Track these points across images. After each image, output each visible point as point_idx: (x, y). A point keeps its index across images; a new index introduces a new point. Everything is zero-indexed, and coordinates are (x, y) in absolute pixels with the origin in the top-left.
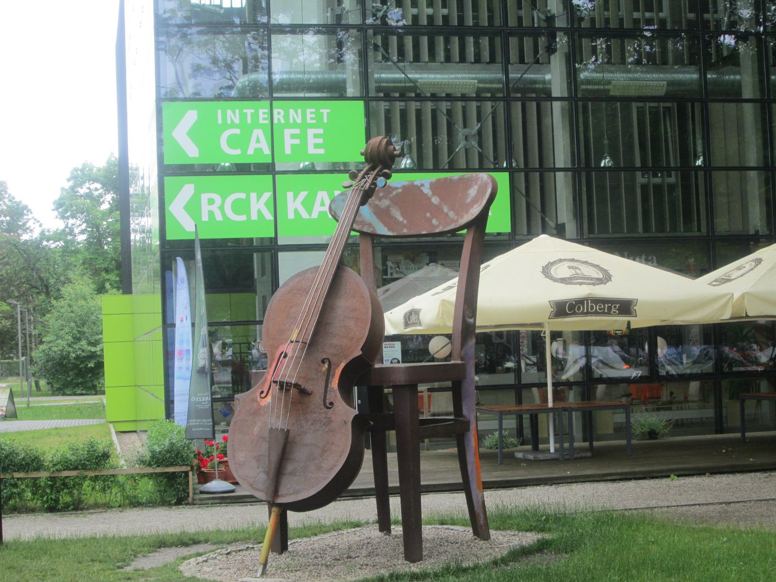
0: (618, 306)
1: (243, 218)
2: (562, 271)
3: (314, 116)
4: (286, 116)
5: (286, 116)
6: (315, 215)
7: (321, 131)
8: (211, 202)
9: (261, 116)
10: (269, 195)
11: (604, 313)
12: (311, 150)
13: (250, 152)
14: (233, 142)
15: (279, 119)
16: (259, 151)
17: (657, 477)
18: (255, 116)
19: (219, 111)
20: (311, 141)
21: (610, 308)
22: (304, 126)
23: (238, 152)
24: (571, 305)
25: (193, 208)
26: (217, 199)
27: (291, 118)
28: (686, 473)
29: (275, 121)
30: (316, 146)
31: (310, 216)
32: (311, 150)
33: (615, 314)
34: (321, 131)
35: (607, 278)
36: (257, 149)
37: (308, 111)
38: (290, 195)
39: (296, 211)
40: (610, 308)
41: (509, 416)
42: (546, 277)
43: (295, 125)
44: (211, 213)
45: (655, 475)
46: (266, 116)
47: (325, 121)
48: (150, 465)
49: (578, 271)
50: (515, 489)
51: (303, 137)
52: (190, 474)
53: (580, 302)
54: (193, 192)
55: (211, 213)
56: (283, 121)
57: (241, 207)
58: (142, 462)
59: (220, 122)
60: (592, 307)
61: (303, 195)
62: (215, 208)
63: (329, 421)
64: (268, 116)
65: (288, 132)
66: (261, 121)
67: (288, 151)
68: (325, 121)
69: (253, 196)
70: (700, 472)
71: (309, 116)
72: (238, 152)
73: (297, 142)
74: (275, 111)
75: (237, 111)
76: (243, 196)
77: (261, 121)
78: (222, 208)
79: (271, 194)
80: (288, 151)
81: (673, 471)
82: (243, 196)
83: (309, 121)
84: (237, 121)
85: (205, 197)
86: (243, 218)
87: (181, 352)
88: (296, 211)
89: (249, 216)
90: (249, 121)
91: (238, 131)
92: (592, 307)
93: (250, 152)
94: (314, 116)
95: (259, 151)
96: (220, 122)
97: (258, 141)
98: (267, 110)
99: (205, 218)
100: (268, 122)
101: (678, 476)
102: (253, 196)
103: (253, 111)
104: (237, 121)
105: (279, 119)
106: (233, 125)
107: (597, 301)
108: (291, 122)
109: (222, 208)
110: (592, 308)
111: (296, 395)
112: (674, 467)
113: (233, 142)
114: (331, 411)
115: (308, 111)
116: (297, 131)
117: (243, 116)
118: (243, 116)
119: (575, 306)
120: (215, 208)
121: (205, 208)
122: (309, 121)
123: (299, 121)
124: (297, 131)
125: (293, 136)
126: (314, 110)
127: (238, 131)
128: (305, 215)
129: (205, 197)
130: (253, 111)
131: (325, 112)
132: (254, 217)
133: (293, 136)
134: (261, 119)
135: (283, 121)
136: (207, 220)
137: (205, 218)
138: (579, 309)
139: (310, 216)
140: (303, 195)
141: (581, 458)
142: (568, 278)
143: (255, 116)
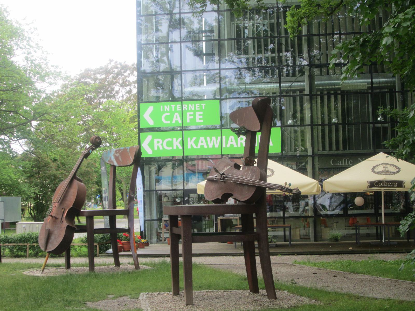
0: (397, 183)
1: (170, 148)
2: (380, 169)
3: (199, 107)
4: (188, 107)
5: (188, 107)
6: (199, 147)
7: (202, 113)
8: (158, 142)
9: (178, 108)
10: (180, 139)
11: (391, 186)
12: (198, 121)
13: (174, 122)
14: (166, 118)
15: (185, 109)
16: (177, 122)
17: (275, 255)
18: (175, 108)
19: (162, 106)
20: (198, 117)
21: (393, 185)
22: (195, 111)
23: (169, 122)
24: (377, 182)
25: (151, 145)
26: (160, 141)
27: (190, 107)
28: (287, 254)
29: (183, 109)
30: (200, 119)
31: (197, 147)
32: (198, 121)
33: (396, 187)
34: (202, 113)
35: (399, 170)
36: (176, 121)
37: (197, 105)
38: (189, 139)
39: (191, 145)
40: (393, 185)
41: (363, 228)
42: (272, 170)
43: (191, 111)
44: (158, 147)
45: (274, 254)
46: (180, 108)
47: (203, 109)
48: (84, 242)
49: (387, 169)
50: (215, 257)
51: (194, 115)
52: (98, 246)
53: (381, 182)
54: (151, 138)
55: (158, 147)
56: (186, 109)
57: (170, 144)
58: (82, 241)
59: (162, 111)
60: (386, 184)
61: (194, 139)
62: (159, 145)
63: (61, 227)
64: (180, 107)
65: (188, 114)
66: (178, 110)
67: (188, 121)
68: (203, 109)
69: (175, 139)
70: (293, 254)
71: (197, 107)
72: (169, 122)
73: (192, 117)
74: (183, 105)
75: (169, 106)
76: (170, 140)
77: (178, 110)
78: (162, 144)
79: (181, 138)
80: (188, 121)
81: (280, 253)
82: (170, 140)
83: (197, 109)
84: (168, 110)
85: (156, 140)
86: (170, 148)
87: (139, 201)
88: (191, 145)
89: (173, 148)
90: (173, 110)
91: (169, 114)
92: (386, 184)
93: (174, 122)
94: (199, 107)
95: (177, 122)
96: (162, 111)
97: (177, 118)
98: (180, 105)
99: (156, 148)
100: (180, 110)
101: (282, 255)
102: (175, 139)
103: (175, 106)
104: (168, 110)
105: (185, 109)
106: (167, 112)
107: (388, 181)
108: (190, 109)
109: (162, 144)
110: (386, 184)
111: (55, 219)
112: (280, 251)
113: (166, 118)
114: (60, 223)
115: (197, 105)
116: (192, 113)
117: (171, 108)
118: (171, 108)
119: (379, 183)
120: (159, 145)
121: (156, 145)
122: (197, 109)
123: (193, 109)
124: (192, 113)
125: (190, 115)
126: (199, 104)
127: (169, 114)
128: (195, 147)
129: (156, 140)
130: (175, 106)
131: (203, 105)
132: (175, 148)
133: (190, 115)
134: (197, 108)
135: (186, 109)
136: (175, 148)
137: (156, 148)
138: (380, 184)
139: (197, 147)
140: (194, 139)
141: (368, 245)
142: (381, 172)
143: (175, 108)
